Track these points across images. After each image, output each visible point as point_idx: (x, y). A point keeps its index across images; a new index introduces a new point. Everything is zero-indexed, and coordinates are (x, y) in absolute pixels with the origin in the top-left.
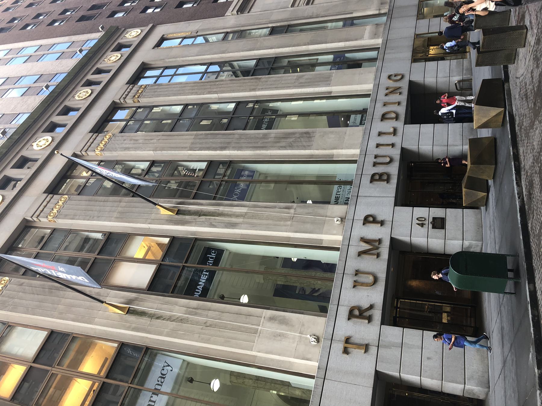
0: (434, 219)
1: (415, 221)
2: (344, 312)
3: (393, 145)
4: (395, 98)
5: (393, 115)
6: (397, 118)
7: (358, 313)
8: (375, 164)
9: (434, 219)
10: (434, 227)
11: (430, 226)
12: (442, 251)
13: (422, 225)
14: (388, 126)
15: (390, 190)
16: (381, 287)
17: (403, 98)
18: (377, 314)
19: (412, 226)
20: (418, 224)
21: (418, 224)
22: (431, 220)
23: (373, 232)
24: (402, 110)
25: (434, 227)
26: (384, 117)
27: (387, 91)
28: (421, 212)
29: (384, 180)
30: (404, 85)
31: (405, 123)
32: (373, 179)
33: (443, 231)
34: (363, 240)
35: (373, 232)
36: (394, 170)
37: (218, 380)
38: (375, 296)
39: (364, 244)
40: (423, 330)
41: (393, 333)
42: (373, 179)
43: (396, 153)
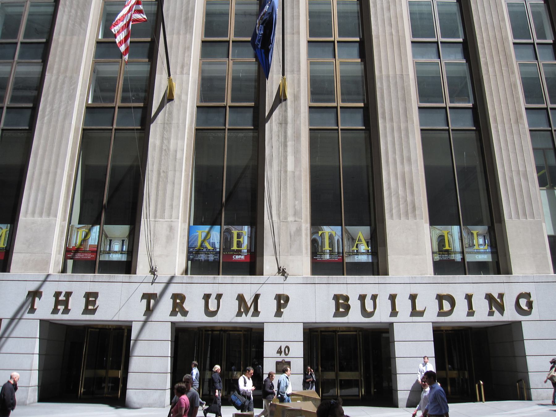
2: (444, 290)
3: (394, 313)
6: (440, 314)
7: (179, 301)
8: (362, 298)
10: (277, 363)
13: (280, 352)
14: (428, 303)
15: (324, 314)
18: (179, 318)
19: (284, 341)
20: (280, 348)
21: (280, 348)
22: (287, 360)
23: (267, 307)
24: (459, 316)
25: (277, 363)
27: (496, 296)
28: (297, 351)
29: (337, 308)
30: (510, 314)
35: (267, 307)
36: (355, 317)
38: (196, 315)
41: (167, 333)
43: (382, 316)
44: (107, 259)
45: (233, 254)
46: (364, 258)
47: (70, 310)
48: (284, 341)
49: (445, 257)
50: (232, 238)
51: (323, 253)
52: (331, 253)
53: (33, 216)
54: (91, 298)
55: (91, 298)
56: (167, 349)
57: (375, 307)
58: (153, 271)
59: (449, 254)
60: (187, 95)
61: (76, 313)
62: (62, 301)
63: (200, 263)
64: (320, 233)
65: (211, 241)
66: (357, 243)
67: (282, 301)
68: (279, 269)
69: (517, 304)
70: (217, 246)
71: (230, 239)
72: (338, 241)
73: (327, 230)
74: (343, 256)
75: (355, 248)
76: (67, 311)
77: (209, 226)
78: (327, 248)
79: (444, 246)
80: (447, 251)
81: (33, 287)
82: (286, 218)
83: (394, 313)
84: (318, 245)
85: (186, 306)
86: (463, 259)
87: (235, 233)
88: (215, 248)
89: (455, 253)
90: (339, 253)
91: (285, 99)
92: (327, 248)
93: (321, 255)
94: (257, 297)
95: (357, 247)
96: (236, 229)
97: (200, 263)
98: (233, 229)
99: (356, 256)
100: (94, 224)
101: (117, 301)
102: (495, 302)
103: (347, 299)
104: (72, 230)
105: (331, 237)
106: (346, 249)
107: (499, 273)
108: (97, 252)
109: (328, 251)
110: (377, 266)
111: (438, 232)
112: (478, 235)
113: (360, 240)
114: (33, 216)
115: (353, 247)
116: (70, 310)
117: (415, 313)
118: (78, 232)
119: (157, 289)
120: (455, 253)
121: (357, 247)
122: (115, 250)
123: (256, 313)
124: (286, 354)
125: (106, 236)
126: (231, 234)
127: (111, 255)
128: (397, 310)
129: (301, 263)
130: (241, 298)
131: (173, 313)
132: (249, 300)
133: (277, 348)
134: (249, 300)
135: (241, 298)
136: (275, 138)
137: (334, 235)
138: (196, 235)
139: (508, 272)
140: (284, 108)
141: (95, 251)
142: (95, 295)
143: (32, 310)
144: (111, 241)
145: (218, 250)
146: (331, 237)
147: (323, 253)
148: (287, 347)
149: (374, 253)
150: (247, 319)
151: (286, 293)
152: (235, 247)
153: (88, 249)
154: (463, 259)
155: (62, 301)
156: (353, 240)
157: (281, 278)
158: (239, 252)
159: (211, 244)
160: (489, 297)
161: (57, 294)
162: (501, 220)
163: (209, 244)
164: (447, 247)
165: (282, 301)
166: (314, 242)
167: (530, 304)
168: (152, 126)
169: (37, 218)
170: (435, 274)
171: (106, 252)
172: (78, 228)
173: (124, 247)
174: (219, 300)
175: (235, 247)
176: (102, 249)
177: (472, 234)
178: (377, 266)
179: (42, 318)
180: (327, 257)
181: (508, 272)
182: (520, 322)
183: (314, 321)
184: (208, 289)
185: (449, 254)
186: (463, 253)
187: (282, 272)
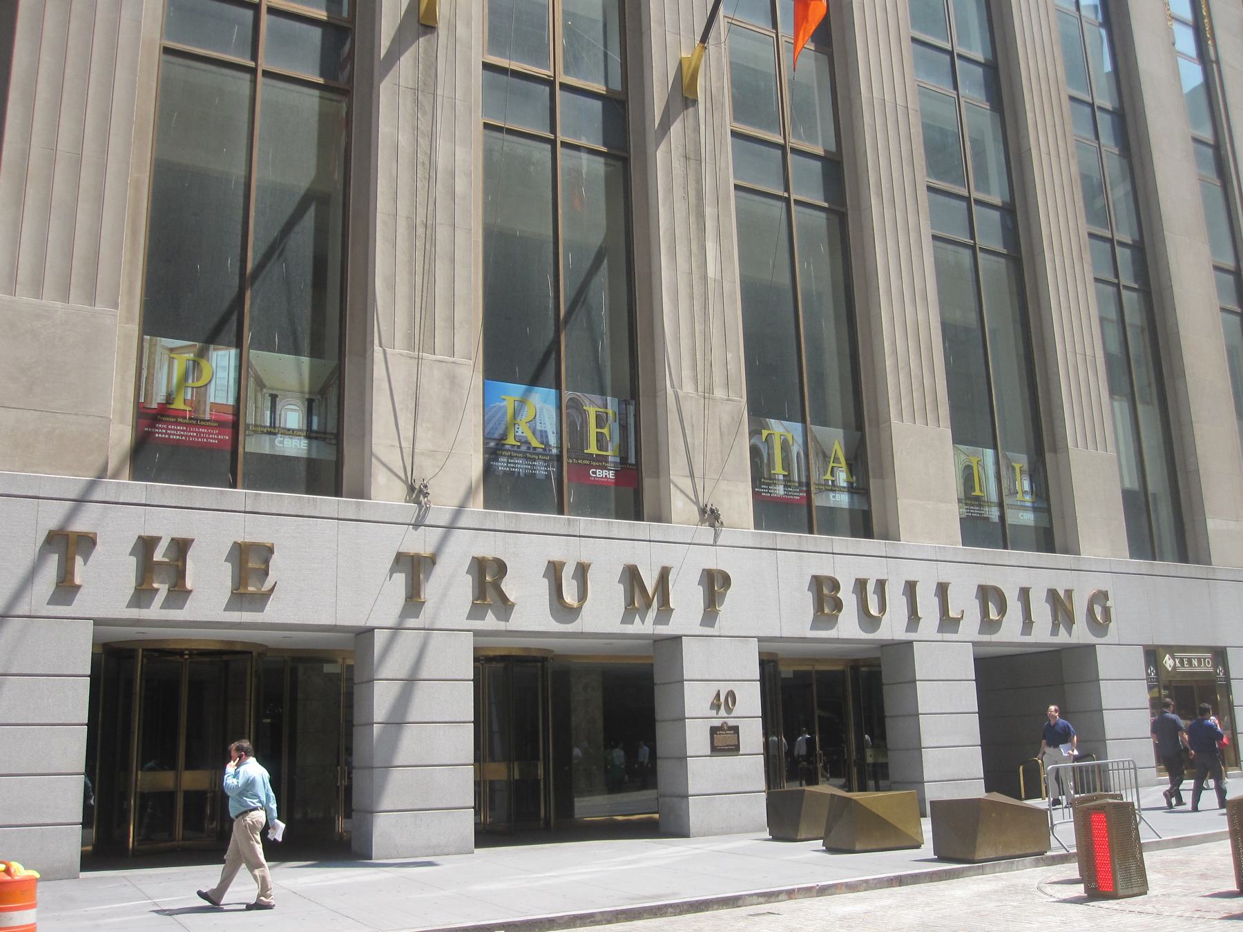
0: (735, 729)
1: (724, 688)
2: (488, 547)
3: (914, 618)
4: (1042, 611)
5: (994, 615)
7: (488, 578)
9: (735, 729)
10: (714, 731)
11: (717, 723)
12: (658, 717)
13: (716, 706)
14: (964, 602)
15: (793, 621)
16: (551, 625)
17: (1043, 634)
18: (490, 622)
20: (718, 695)
21: (718, 695)
22: (731, 722)
23: (687, 598)
24: (1010, 632)
25: (714, 731)
26: (989, 595)
27: (1062, 594)
28: (750, 701)
30: (1080, 634)
31: (975, 644)
32: (818, 584)
33: (709, 753)
34: (664, 574)
35: (687, 598)
36: (848, 627)
37: (155, 559)
38: (530, 616)
39: (656, 575)
40: (476, 680)
42: (818, 584)
43: (893, 627)
44: (267, 450)
45: (591, 466)
46: (295, 447)
47: (79, 587)
48: (717, 682)
49: (976, 511)
50: (585, 423)
51: (772, 481)
52: (788, 480)
53: (38, 294)
54: (250, 563)
55: (250, 563)
56: (76, 700)
57: (883, 608)
58: (417, 493)
59: (980, 506)
60: (469, 25)
61: (205, 605)
62: (161, 566)
63: (513, 481)
64: (765, 433)
65: (538, 428)
66: (831, 464)
67: (715, 585)
68: (703, 511)
69: (1090, 611)
70: (553, 440)
71: (582, 426)
72: (798, 454)
73: (778, 428)
74: (809, 492)
75: (828, 476)
76: (179, 593)
77: (523, 387)
78: (779, 470)
79: (973, 488)
80: (978, 498)
81: (51, 517)
82: (711, 391)
83: (914, 618)
84: (762, 461)
85: (508, 586)
86: (1002, 517)
87: (592, 411)
88: (547, 444)
89: (989, 504)
90: (800, 483)
91: (695, 102)
92: (779, 470)
93: (769, 484)
94: (664, 574)
95: (832, 474)
96: (592, 403)
97: (513, 481)
98: (587, 402)
99: (832, 495)
100: (213, 338)
101: (321, 571)
102: (1060, 605)
103: (835, 586)
104: (152, 353)
105: (785, 447)
106: (814, 479)
107: (868, 533)
108: (235, 425)
109: (781, 477)
110: (328, 470)
111: (963, 457)
112: (1022, 472)
113: (836, 460)
114: (38, 294)
115: (825, 473)
116: (79, 587)
117: (948, 623)
118: (171, 360)
119: (420, 543)
120: (989, 504)
121: (832, 474)
122: (288, 426)
123: (665, 611)
124: (729, 710)
125: (260, 384)
126: (583, 414)
127: (279, 438)
128: (672, 606)
129: (738, 501)
130: (632, 576)
131: (477, 611)
132: (650, 582)
133: (711, 698)
134: (650, 582)
135: (632, 576)
136: (678, 192)
137: (790, 441)
138: (500, 408)
139: (1071, 548)
140: (690, 122)
141: (234, 423)
142: (266, 552)
143: (66, 588)
144: (274, 398)
145: (554, 451)
146: (785, 447)
147: (772, 481)
148: (731, 694)
149: (859, 489)
150: (646, 626)
151: (721, 566)
152: (593, 449)
153: (208, 417)
154: (1002, 517)
155: (161, 566)
156: (826, 457)
157: (706, 533)
158: (601, 461)
159: (538, 434)
160: (1053, 595)
161: (146, 545)
162: (1059, 447)
163: (534, 433)
164: (977, 493)
165: (715, 585)
166: (755, 451)
167: (1106, 612)
168: (385, 90)
169: (50, 302)
170: (758, 525)
171: (259, 430)
172: (172, 350)
173: (315, 419)
174: (572, 580)
175: (593, 449)
176: (251, 420)
177: (1014, 469)
178: (328, 470)
179: (762, 634)
180: (780, 490)
181: (1071, 548)
182: (1093, 646)
183: (778, 635)
184: (558, 549)
185: (980, 506)
186: (1001, 505)
187: (710, 516)
